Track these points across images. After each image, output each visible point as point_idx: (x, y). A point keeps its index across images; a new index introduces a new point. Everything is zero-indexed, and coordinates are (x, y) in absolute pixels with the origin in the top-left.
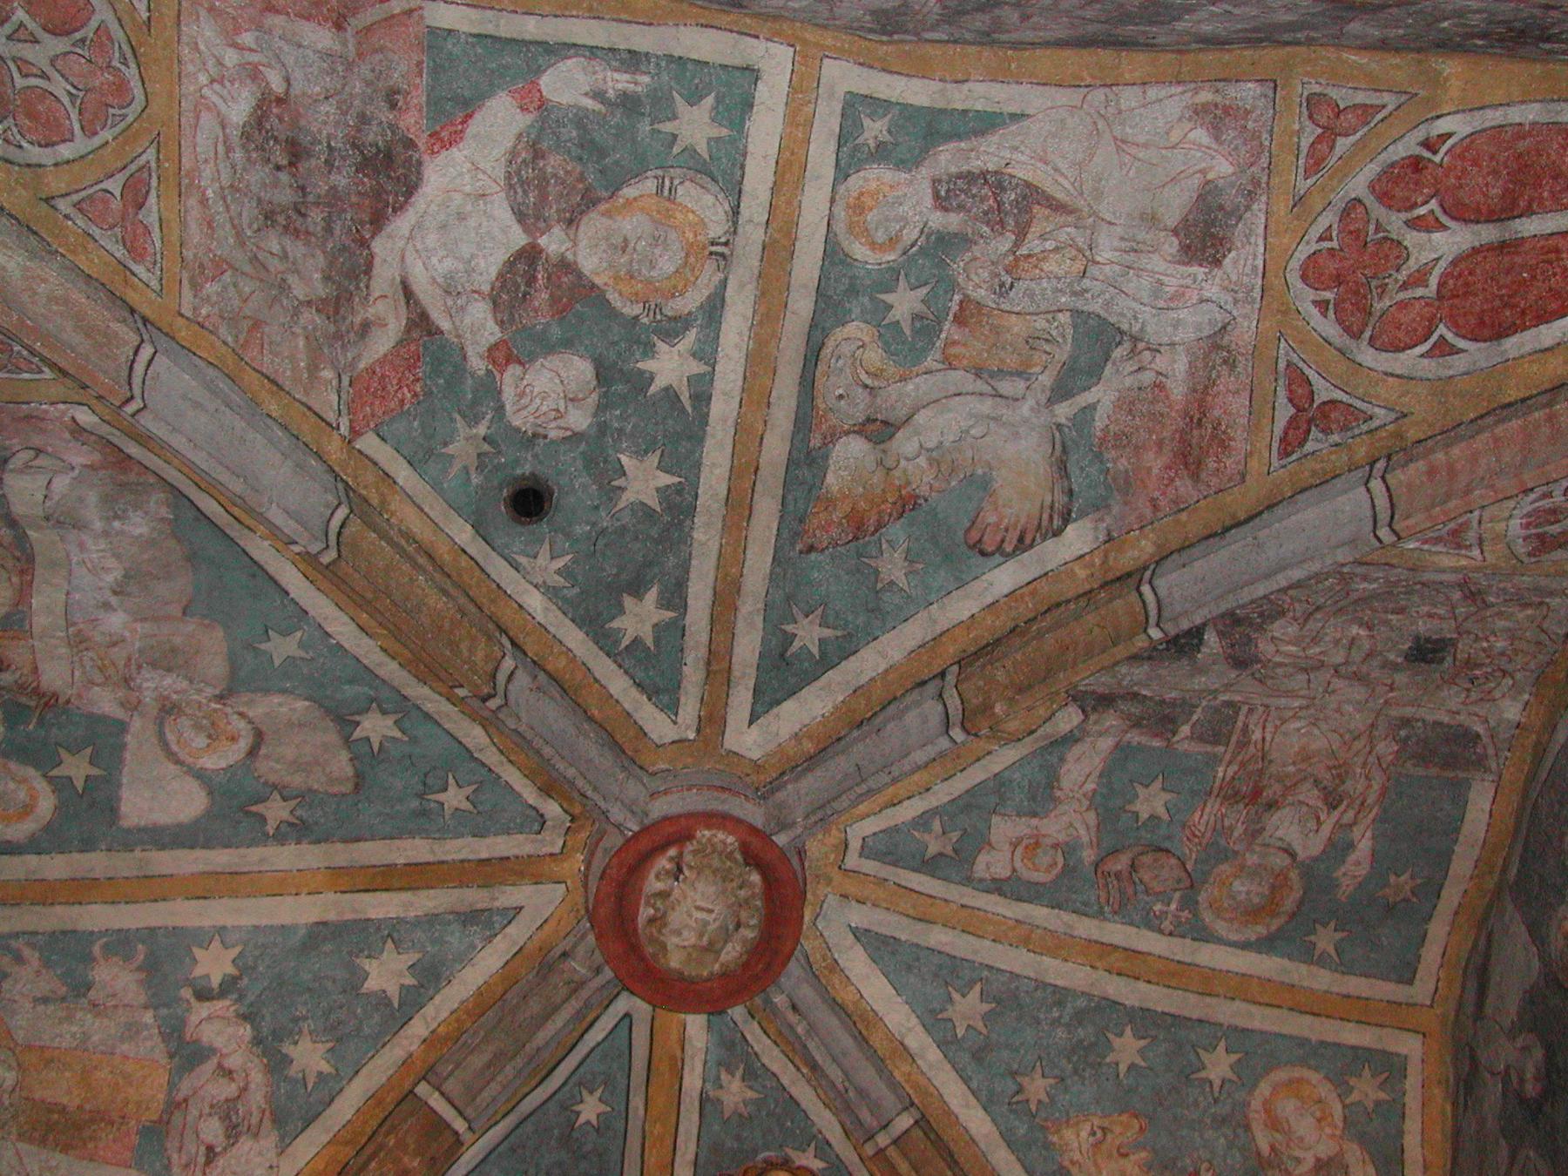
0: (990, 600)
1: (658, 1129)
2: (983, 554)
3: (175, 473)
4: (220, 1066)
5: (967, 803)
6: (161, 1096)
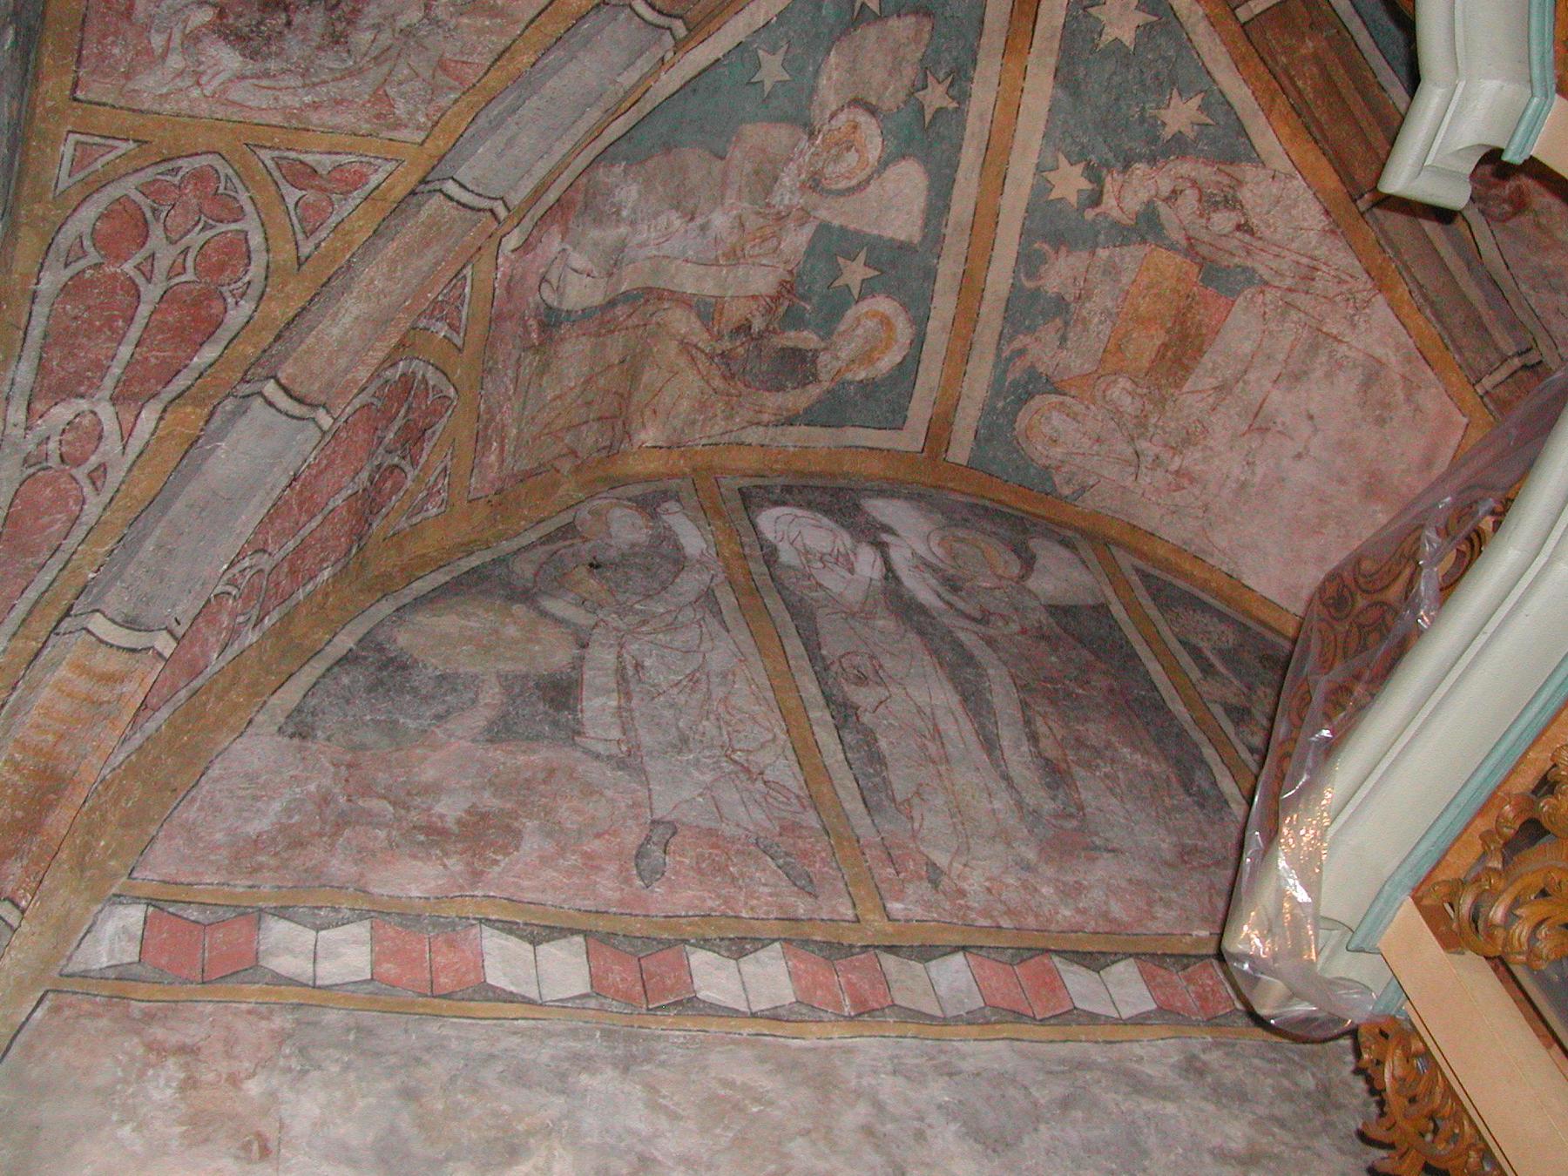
3: (579, 159)
4: (1166, 200)
6: (1179, 259)
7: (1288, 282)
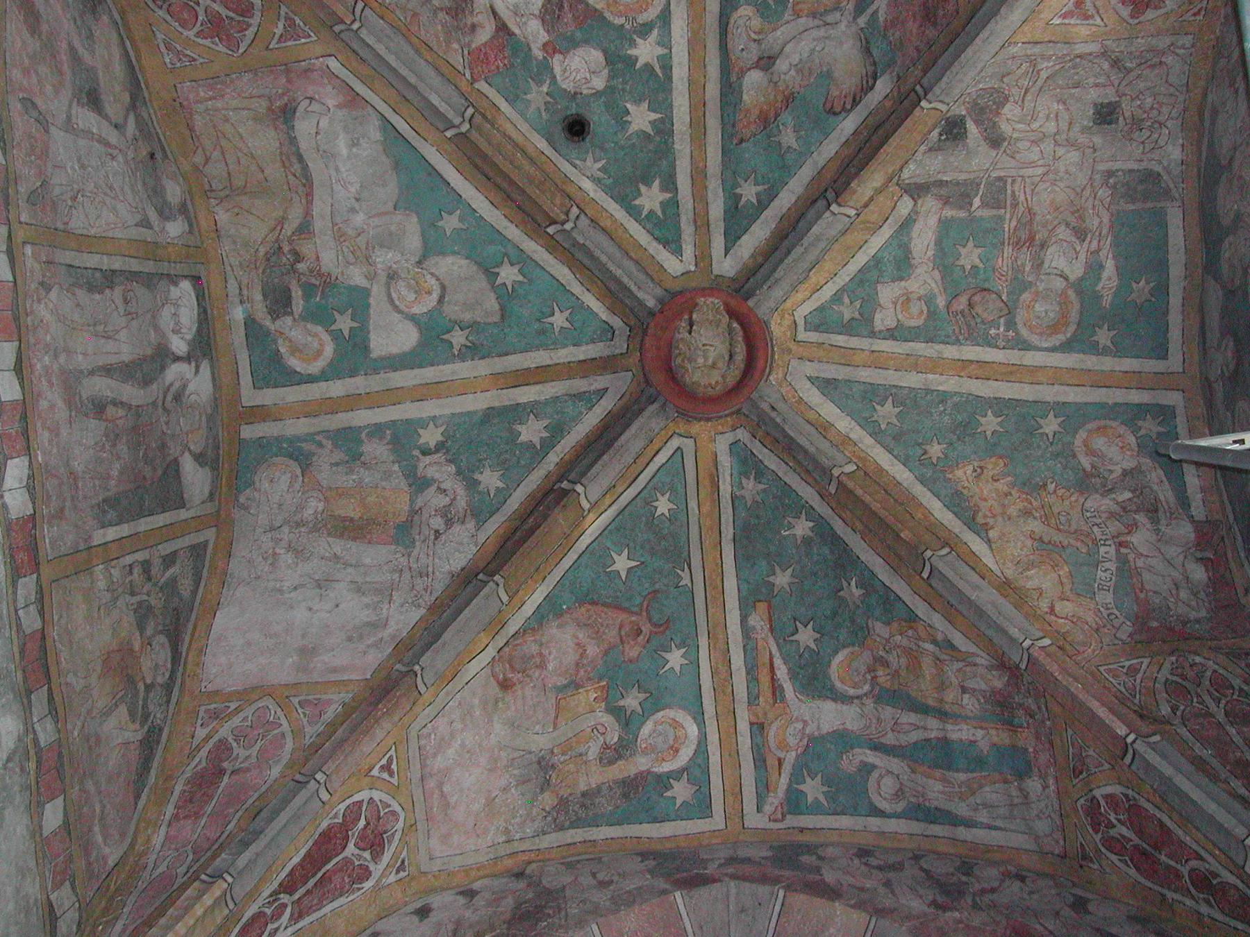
0: (844, 140)
1: (708, 523)
2: (835, 114)
4: (439, 488)
5: (861, 277)
6: (406, 508)
7: (415, 566)
